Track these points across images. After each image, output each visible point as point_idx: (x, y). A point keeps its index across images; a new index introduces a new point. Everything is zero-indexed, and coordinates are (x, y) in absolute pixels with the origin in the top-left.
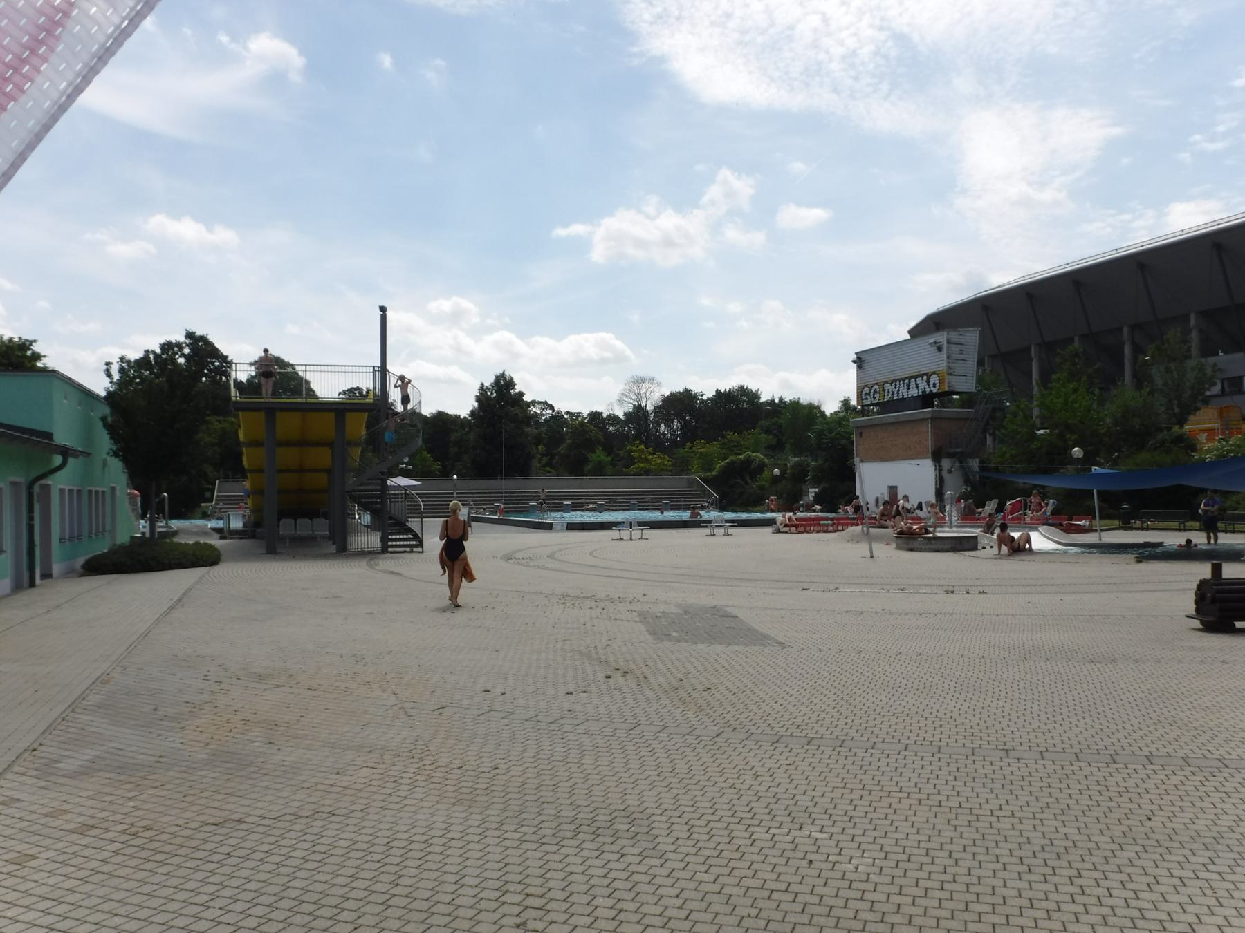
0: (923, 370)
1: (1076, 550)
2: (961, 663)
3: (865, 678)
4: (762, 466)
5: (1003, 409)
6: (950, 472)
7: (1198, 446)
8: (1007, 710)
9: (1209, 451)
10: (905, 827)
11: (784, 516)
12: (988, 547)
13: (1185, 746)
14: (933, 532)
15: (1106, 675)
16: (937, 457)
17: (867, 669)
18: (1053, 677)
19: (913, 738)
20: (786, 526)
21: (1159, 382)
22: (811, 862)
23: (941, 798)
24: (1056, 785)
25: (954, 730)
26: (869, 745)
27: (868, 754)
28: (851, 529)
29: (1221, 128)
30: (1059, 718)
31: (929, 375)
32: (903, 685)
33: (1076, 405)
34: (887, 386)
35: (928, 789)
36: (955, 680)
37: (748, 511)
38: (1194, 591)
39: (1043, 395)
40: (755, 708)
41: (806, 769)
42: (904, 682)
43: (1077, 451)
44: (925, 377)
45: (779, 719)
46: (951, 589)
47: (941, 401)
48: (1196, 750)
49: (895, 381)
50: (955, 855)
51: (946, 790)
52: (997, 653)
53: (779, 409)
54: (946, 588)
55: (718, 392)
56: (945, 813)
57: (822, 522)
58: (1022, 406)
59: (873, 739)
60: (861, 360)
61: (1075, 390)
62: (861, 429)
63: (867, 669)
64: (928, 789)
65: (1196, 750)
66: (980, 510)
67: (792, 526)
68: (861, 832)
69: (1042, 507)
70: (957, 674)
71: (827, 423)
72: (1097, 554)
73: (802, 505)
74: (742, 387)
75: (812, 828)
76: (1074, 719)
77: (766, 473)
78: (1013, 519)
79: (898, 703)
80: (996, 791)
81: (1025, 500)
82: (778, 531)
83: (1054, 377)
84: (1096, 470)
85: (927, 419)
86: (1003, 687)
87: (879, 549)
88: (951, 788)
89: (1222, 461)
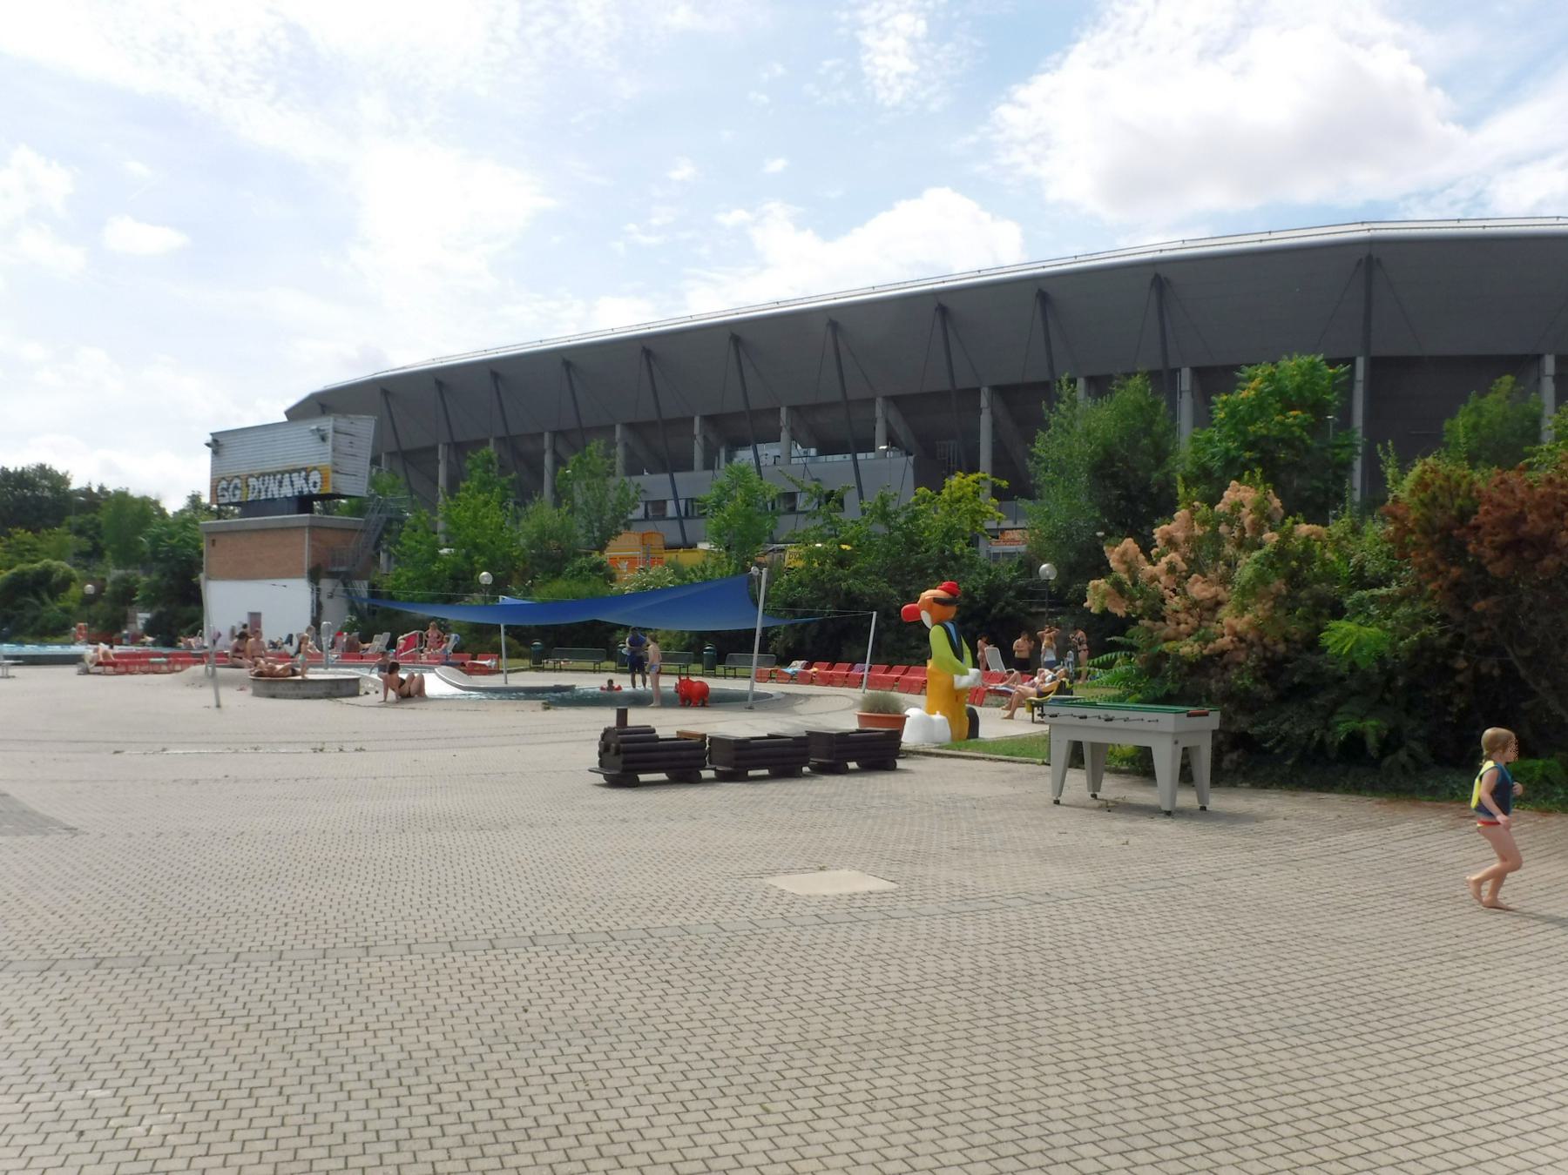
0: (301, 464)
1: (475, 695)
2: (322, 841)
3: (189, 869)
4: (67, 582)
5: (401, 521)
6: (331, 597)
7: (618, 576)
8: (372, 896)
9: (628, 582)
10: (223, 1064)
11: (96, 651)
12: (372, 693)
13: (572, 921)
14: (302, 674)
15: (494, 844)
16: (314, 576)
17: (193, 857)
18: (433, 852)
19: (247, 945)
20: (99, 664)
21: (579, 501)
22: (81, 1133)
23: (276, 1018)
24: (445, 982)
25: (303, 928)
26: (187, 958)
27: (183, 972)
28: (193, 668)
29: (655, 222)
30: (434, 902)
31: (307, 471)
32: (241, 875)
33: (487, 521)
34: (252, 481)
35: (262, 1009)
36: (312, 863)
37: (42, 643)
38: (597, 743)
39: (448, 506)
40: (19, 925)
41: (166, 998)
42: (244, 870)
43: (485, 577)
44: (303, 474)
45: (54, 937)
46: (319, 746)
47: (324, 505)
48: (584, 923)
49: (263, 475)
50: (377, 1084)
51: (284, 1007)
52: (369, 826)
53: (93, 501)
54: (313, 746)
56: (280, 1037)
57: (152, 660)
58: (423, 518)
59: (192, 951)
60: (217, 444)
61: (486, 504)
62: (214, 536)
63: (193, 857)
64: (262, 1009)
65: (584, 923)
66: (367, 645)
67: (108, 664)
68: (220, 1076)
69: (442, 642)
70: (316, 855)
71: (166, 525)
73: (126, 636)
74: (42, 467)
75: (89, 1085)
76: (452, 902)
77: (74, 590)
78: (407, 657)
79: (232, 899)
80: (372, 999)
81: (421, 635)
82: (87, 672)
83: (462, 485)
84: (504, 600)
85: (303, 527)
86: (371, 867)
87: (231, 696)
88: (291, 1004)
89: (642, 594)
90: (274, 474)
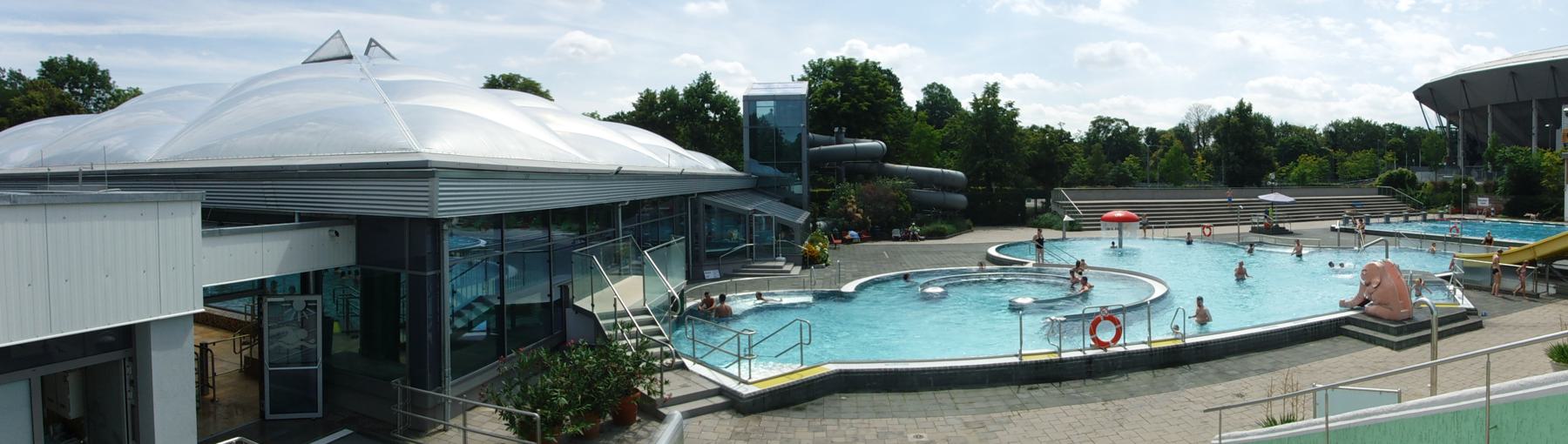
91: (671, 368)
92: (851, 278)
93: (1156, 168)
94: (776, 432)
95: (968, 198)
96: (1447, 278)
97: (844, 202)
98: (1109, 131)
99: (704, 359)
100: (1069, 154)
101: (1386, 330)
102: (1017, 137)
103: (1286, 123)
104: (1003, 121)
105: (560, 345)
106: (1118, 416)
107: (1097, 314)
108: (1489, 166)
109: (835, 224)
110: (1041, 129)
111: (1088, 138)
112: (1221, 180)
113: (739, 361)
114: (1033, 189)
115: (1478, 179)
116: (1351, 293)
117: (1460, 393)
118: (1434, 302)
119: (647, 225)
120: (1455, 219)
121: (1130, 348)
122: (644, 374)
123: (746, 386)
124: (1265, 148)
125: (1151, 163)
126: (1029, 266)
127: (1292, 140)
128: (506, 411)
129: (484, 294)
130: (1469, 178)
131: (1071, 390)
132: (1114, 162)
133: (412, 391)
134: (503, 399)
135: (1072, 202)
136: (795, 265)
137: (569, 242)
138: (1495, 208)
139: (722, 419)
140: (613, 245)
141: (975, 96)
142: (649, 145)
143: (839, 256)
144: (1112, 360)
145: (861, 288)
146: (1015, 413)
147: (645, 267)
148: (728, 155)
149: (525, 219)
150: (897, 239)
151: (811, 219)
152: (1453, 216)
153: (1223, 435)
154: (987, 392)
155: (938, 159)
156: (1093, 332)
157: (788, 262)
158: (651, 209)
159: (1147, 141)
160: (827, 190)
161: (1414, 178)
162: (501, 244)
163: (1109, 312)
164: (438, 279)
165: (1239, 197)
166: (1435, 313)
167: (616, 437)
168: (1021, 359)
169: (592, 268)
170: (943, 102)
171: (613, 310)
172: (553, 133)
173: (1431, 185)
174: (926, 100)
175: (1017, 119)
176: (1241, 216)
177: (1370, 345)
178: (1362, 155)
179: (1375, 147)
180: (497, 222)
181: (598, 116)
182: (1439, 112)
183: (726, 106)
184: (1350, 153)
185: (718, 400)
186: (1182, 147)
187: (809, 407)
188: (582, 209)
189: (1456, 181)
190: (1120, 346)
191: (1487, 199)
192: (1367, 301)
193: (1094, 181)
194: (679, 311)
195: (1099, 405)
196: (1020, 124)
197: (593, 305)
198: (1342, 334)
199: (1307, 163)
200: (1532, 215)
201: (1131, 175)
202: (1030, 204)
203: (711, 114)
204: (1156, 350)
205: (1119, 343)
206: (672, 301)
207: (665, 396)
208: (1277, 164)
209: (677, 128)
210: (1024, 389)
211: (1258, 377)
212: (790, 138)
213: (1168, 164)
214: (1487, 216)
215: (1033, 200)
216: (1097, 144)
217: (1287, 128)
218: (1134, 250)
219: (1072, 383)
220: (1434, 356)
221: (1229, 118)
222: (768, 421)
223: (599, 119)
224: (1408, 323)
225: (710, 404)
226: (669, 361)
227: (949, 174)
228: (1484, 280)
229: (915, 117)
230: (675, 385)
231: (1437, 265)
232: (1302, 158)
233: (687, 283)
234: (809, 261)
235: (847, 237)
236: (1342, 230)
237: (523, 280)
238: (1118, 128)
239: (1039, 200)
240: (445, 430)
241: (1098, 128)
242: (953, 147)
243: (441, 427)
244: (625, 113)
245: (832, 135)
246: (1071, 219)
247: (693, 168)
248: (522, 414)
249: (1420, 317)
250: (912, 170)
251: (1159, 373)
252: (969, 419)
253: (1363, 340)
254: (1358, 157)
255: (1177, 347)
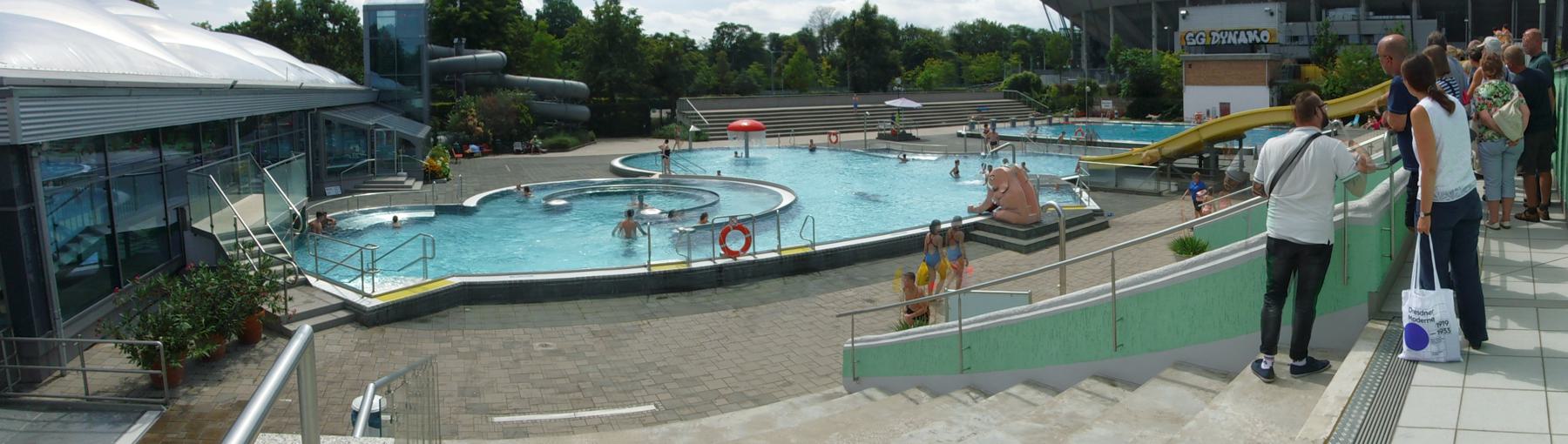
44: (1256, 32)
55: (868, 13)
72: (826, 151)
90: (1233, 32)
91: (294, 285)
92: (472, 193)
93: (780, 74)
94: (400, 343)
95: (590, 107)
96: (1073, 181)
97: (465, 115)
98: (733, 37)
99: (327, 276)
100: (695, 62)
101: (1014, 234)
102: (640, 45)
103: (912, 26)
104: (626, 29)
105: (180, 270)
106: (749, 323)
107: (727, 223)
108: (1112, 69)
109: (456, 139)
110: (666, 37)
111: (712, 45)
112: (847, 85)
113: (362, 276)
114: (658, 99)
115: (1102, 81)
116: (979, 198)
117: (1089, 291)
118: (1062, 205)
119: (266, 142)
120: (1079, 122)
121: (760, 257)
122: (268, 292)
123: (369, 299)
124: (891, 52)
125: (775, 69)
126: (656, 177)
127: (917, 44)
128: (127, 344)
129: (92, 224)
130: (1093, 81)
131: (703, 299)
132: (739, 70)
133: (17, 342)
134: (122, 332)
135: (698, 112)
136: (417, 180)
137: (183, 162)
138: (1118, 110)
139: (346, 332)
140: (231, 163)
141: (596, 3)
142: (266, 58)
143: (460, 171)
144: (741, 269)
145: (482, 202)
146: (645, 322)
147: (265, 185)
148: (348, 68)
149: (134, 139)
150: (518, 152)
151: (432, 134)
152: (1078, 120)
153: (855, 339)
154: (614, 302)
155: (559, 70)
156: (722, 241)
157: (409, 177)
158: (270, 125)
159: (771, 46)
160: (447, 104)
161: (1039, 82)
162: (105, 168)
163: (739, 221)
164: (32, 215)
165: (865, 103)
166: (1062, 216)
167: (242, 356)
168: (649, 269)
169: (210, 189)
170: (563, 10)
171: (233, 229)
172: (160, 45)
173: (1056, 88)
174: (545, 8)
175: (641, 27)
176: (868, 123)
177: (999, 249)
178: (987, 58)
179: (1000, 50)
180: (99, 144)
181: (210, 27)
182: (1063, 13)
183: (345, 17)
184: (974, 55)
185: (342, 314)
186: (805, 53)
187: (434, 319)
188: (195, 126)
189: (1080, 84)
190: (750, 254)
191: (1111, 102)
192: (995, 206)
193: (720, 90)
194: (301, 229)
195: (730, 313)
196: (643, 32)
197: (212, 226)
198: (971, 240)
199: (933, 68)
200: (1153, 117)
201: (755, 83)
202: (655, 115)
203: (330, 25)
204: (786, 257)
205: (748, 252)
206: (294, 218)
207: (289, 313)
208: (903, 68)
209: (295, 39)
210: (653, 298)
211: (888, 282)
212: (410, 50)
213: (793, 70)
214: (1111, 119)
215: (658, 111)
216: (722, 52)
217: (912, 31)
218: (759, 159)
219: (703, 293)
220: (1063, 257)
221: (854, 21)
222: (391, 332)
223: (211, 30)
224: (1037, 227)
225: (335, 318)
226: (292, 278)
227: (572, 85)
228: (1110, 182)
229: (536, 26)
230: (298, 302)
231: (1062, 167)
232: (928, 63)
233: (309, 200)
234: (430, 176)
235: (468, 151)
236: (969, 136)
237: (134, 206)
238: (742, 34)
239: (664, 111)
240: (62, 375)
241: (722, 35)
242: (576, 57)
243: (58, 373)
244: (240, 23)
245: (452, 47)
246: (697, 129)
247: (312, 81)
248: (144, 345)
249: (1047, 220)
250: (533, 81)
251: (789, 280)
252: (596, 327)
253: (992, 245)
254: (983, 60)
255: (807, 254)
